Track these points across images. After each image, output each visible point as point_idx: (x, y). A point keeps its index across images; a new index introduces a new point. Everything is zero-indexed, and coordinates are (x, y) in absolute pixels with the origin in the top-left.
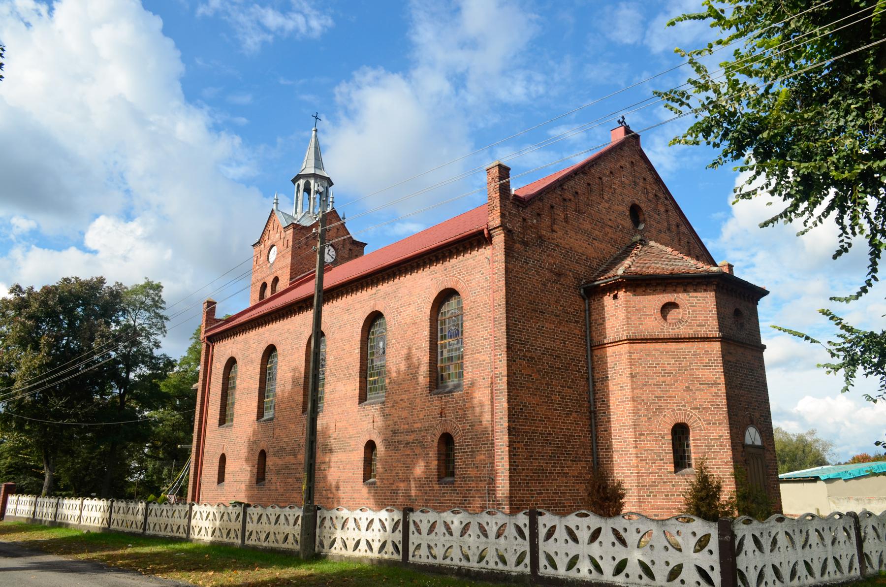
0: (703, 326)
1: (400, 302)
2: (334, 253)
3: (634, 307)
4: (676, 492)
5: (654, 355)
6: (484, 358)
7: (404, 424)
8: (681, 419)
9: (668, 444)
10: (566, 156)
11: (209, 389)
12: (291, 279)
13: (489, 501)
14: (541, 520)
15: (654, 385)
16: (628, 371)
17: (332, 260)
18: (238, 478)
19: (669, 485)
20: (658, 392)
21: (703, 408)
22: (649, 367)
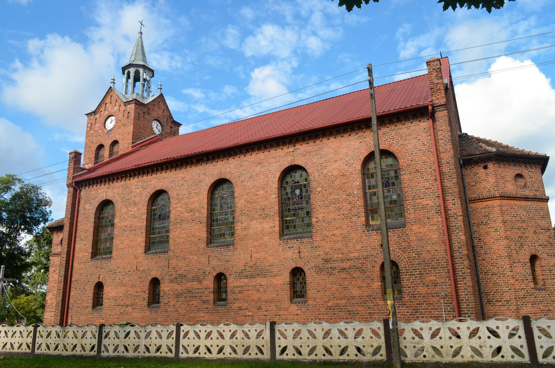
0: (538, 191)
1: (324, 159)
2: (160, 128)
3: (500, 175)
4: (537, 302)
5: (515, 209)
6: (427, 202)
7: (338, 254)
8: (534, 252)
9: (529, 269)
10: (192, 106)
11: (76, 226)
12: (133, 143)
13: (445, 311)
14: (182, 328)
15: (517, 229)
16: (500, 219)
17: (159, 133)
18: (122, 303)
19: (533, 297)
20: (520, 234)
21: (544, 245)
22: (513, 216)
